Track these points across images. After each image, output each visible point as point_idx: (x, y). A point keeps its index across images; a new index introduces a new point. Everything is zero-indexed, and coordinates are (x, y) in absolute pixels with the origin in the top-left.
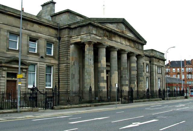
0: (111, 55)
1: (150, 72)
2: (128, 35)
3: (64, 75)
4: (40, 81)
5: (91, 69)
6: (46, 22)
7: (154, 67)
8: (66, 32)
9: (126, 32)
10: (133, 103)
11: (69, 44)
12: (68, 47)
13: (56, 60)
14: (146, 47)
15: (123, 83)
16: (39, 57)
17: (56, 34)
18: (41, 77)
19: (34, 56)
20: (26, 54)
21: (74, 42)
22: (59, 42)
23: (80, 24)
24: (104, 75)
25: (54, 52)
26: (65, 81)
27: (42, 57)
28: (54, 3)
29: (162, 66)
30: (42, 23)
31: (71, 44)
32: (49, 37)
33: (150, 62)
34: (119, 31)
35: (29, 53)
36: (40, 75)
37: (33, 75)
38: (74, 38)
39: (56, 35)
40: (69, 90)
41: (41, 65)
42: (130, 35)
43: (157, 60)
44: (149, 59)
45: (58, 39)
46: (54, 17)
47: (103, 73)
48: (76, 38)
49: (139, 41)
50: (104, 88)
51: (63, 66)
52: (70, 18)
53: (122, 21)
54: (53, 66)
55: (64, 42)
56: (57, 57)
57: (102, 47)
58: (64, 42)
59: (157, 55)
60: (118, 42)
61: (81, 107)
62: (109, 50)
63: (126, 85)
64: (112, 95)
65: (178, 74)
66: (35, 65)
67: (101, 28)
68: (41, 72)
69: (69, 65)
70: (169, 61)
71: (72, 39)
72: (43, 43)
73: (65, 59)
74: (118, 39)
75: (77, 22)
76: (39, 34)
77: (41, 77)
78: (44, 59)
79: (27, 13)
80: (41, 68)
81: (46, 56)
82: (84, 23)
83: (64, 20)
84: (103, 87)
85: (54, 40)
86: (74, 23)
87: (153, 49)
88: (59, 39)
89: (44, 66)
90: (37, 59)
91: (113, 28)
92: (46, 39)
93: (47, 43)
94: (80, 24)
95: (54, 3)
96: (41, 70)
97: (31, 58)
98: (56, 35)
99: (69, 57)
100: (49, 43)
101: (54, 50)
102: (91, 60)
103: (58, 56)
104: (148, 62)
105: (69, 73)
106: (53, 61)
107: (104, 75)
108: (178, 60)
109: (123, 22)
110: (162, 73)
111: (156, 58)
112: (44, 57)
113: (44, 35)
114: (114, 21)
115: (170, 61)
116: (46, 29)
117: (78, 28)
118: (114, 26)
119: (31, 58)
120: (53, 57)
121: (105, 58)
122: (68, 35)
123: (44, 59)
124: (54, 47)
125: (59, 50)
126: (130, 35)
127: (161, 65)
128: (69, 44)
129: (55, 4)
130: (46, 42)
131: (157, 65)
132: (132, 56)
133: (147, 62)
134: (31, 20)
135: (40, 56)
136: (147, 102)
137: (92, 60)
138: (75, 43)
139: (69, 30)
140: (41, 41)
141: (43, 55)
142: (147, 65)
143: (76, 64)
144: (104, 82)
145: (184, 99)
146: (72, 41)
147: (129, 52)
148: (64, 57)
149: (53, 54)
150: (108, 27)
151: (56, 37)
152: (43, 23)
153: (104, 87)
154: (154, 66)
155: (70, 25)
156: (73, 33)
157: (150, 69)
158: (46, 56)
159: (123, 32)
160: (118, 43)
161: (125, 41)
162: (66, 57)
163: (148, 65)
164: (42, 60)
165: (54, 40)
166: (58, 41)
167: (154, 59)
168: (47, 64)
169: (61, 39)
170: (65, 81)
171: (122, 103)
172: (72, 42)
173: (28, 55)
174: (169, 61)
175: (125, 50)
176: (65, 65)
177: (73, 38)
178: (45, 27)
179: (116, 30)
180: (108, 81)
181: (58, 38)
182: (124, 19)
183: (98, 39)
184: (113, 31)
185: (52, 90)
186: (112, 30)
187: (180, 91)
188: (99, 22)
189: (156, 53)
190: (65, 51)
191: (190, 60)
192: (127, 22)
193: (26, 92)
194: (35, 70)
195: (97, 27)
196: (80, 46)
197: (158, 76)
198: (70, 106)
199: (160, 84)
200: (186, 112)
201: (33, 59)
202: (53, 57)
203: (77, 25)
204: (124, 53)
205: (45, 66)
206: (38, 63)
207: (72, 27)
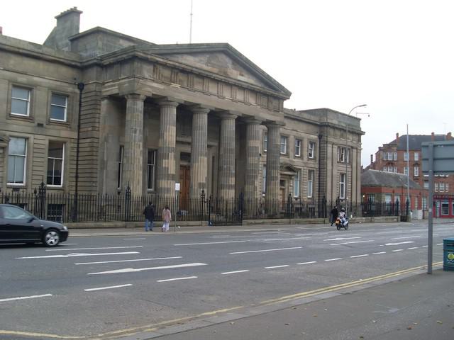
0: (194, 121)
1: (320, 160)
3: (86, 162)
4: (35, 173)
6: (53, 54)
7: (329, 149)
8: (93, 73)
11: (98, 98)
12: (96, 106)
13: (71, 131)
14: (287, 105)
15: (223, 181)
16: (33, 124)
17: (75, 77)
18: (35, 164)
19: (22, 123)
21: (108, 93)
22: (81, 94)
23: (119, 57)
24: (171, 164)
25: (68, 114)
26: (88, 175)
27: (40, 125)
28: (80, 13)
29: (352, 147)
31: (103, 98)
32: (59, 83)
33: (320, 137)
34: (215, 70)
35: (10, 116)
36: (33, 161)
37: (20, 159)
38: (109, 87)
39: (75, 79)
40: (93, 194)
41: (36, 141)
42: (246, 79)
43: (338, 133)
44: (317, 129)
45: (79, 88)
46: (76, 42)
47: (167, 161)
48: (113, 86)
49: (272, 92)
50: (168, 191)
51: (85, 143)
52: (103, 44)
53: (222, 49)
54: (65, 143)
55: (90, 94)
56: (75, 125)
57: (167, 105)
58: (90, 94)
60: (211, 94)
61: (77, 228)
62: (186, 113)
63: (230, 187)
64: (222, 206)
65: (414, 165)
67: (165, 65)
68: (35, 155)
69: (96, 140)
70: (397, 134)
71: (105, 88)
72: (43, 96)
73: (90, 129)
74: (213, 88)
75: (114, 53)
76: (36, 79)
77: (35, 164)
78: (45, 128)
79: (10, 38)
80: (36, 146)
81: (50, 123)
82: (124, 56)
83: (96, 51)
84: (165, 188)
85: (70, 89)
86: (108, 56)
87: (326, 107)
88: (81, 86)
89: (44, 142)
90: (29, 129)
91: (198, 65)
92: (50, 88)
94: (119, 57)
95: (80, 13)
96: (35, 150)
97: (14, 127)
98: (75, 79)
99: (97, 125)
100: (58, 95)
101: (68, 110)
102: (135, 132)
103: (80, 124)
104: (315, 137)
105: (95, 158)
106: (65, 133)
107: (171, 164)
108: (418, 134)
109: (226, 50)
111: (334, 128)
112: (45, 125)
113: (47, 81)
114: (199, 50)
115: (399, 136)
116: (52, 67)
117: (115, 66)
118: (201, 61)
119: (15, 126)
120: (67, 125)
121: (174, 129)
122: (97, 79)
123: (45, 128)
124: (68, 105)
125: (80, 111)
126: (246, 79)
127: (350, 144)
128: (99, 98)
129: (81, 15)
131: (336, 144)
132: (252, 123)
133: (312, 136)
134: (17, 50)
135: (36, 123)
137: (138, 132)
138: (110, 96)
139: (99, 69)
140: (38, 92)
141: (43, 120)
142: (312, 143)
143: (110, 141)
144: (168, 180)
145: (398, 221)
146: (106, 91)
147: (241, 115)
148: (88, 125)
149: (67, 118)
151: (75, 84)
152: (44, 56)
153: (168, 189)
154: (330, 145)
155: (102, 58)
156: (107, 75)
157: (320, 152)
158: (50, 123)
159: (226, 74)
160: (208, 97)
161: (231, 90)
162: (91, 124)
163: (315, 143)
164: (39, 130)
165: (70, 89)
166: (78, 91)
167: (331, 131)
168: (52, 138)
169: (85, 87)
170: (88, 175)
172: (105, 94)
173: (9, 121)
174: (397, 134)
175: (228, 111)
176: (88, 140)
177: (106, 85)
178: (48, 64)
179: (205, 67)
180: (185, 174)
181: (79, 85)
182: (227, 45)
183: (159, 89)
187: (392, 205)
188: (157, 52)
190: (90, 111)
191: (446, 134)
192: (235, 51)
195: (155, 64)
196: (119, 103)
197: (339, 168)
198: (401, 232)
199: (346, 186)
200: (265, 244)
201: (20, 129)
202: (67, 125)
203: (111, 59)
204: (228, 118)
205: (47, 142)
206: (32, 137)
207: (106, 62)
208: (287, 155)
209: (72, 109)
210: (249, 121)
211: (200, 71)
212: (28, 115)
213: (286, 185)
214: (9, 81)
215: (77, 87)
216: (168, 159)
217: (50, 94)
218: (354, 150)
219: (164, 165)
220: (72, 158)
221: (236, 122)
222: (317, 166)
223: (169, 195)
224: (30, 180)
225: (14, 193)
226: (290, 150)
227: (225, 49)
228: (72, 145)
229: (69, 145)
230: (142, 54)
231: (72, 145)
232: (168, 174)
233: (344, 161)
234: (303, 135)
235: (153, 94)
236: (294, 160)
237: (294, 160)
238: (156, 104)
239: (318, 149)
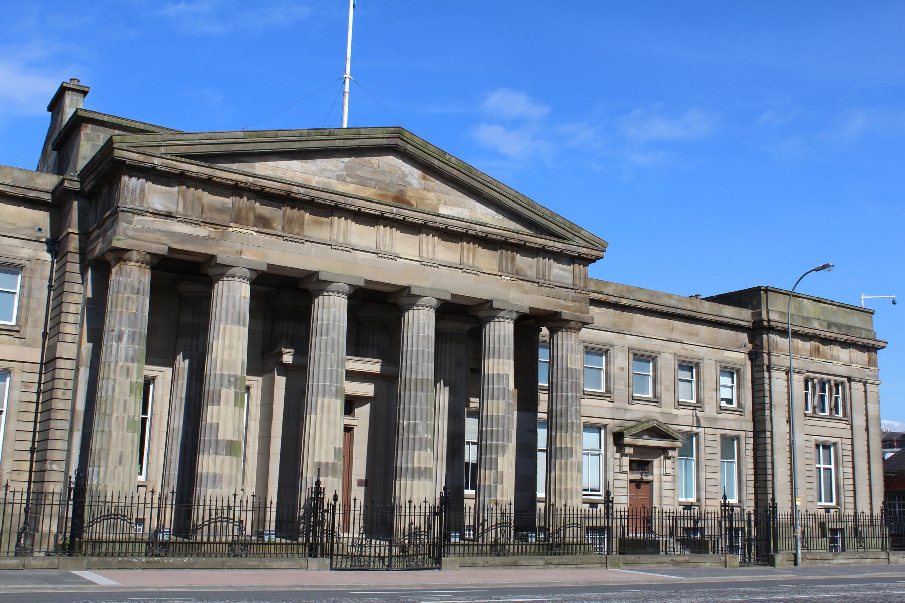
2: (443, 210)
5: (115, 380)
9: (432, 196)
10: (440, 569)
20: (716, 413)
30: (693, 313)
33: (755, 356)
34: (368, 193)
39: (40, 230)
45: (49, 251)
47: (215, 407)
56: (35, 331)
59: (808, 319)
66: (600, 429)
76: (727, 353)
93: (680, 366)
104: (739, 358)
110: (699, 405)
127: (843, 371)
130: (676, 362)
136: (621, 580)
144: (216, 454)
150: (255, 176)
153: (215, 476)
159: (400, 199)
167: (782, 342)
171: (332, 569)
173: (631, 407)
182: (399, 133)
184: (302, 190)
185: (764, 509)
186: (295, 189)
188: (182, 150)
189: (800, 308)
193: (678, 514)
194: (600, 448)
197: (810, 430)
205: (719, 438)
208: (656, 400)
209: (29, 297)
210: (482, 314)
211: (313, 193)
212: (13, 323)
213: (656, 470)
214: (630, 349)
215: (45, 247)
216: (219, 404)
217: (631, 356)
218: (857, 387)
219: (208, 420)
220: (23, 407)
221: (438, 319)
222: (749, 426)
223: (218, 491)
224: (703, 494)
225: (686, 511)
226: (661, 389)
227: (392, 142)
228: (26, 377)
229: (18, 377)
230: (135, 156)
231: (26, 377)
232: (217, 441)
233: (840, 415)
234: (701, 352)
235: (171, 249)
236: (675, 412)
237: (675, 412)
238: (395, 304)
239: (748, 385)
